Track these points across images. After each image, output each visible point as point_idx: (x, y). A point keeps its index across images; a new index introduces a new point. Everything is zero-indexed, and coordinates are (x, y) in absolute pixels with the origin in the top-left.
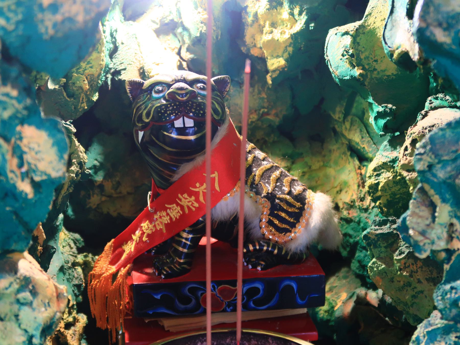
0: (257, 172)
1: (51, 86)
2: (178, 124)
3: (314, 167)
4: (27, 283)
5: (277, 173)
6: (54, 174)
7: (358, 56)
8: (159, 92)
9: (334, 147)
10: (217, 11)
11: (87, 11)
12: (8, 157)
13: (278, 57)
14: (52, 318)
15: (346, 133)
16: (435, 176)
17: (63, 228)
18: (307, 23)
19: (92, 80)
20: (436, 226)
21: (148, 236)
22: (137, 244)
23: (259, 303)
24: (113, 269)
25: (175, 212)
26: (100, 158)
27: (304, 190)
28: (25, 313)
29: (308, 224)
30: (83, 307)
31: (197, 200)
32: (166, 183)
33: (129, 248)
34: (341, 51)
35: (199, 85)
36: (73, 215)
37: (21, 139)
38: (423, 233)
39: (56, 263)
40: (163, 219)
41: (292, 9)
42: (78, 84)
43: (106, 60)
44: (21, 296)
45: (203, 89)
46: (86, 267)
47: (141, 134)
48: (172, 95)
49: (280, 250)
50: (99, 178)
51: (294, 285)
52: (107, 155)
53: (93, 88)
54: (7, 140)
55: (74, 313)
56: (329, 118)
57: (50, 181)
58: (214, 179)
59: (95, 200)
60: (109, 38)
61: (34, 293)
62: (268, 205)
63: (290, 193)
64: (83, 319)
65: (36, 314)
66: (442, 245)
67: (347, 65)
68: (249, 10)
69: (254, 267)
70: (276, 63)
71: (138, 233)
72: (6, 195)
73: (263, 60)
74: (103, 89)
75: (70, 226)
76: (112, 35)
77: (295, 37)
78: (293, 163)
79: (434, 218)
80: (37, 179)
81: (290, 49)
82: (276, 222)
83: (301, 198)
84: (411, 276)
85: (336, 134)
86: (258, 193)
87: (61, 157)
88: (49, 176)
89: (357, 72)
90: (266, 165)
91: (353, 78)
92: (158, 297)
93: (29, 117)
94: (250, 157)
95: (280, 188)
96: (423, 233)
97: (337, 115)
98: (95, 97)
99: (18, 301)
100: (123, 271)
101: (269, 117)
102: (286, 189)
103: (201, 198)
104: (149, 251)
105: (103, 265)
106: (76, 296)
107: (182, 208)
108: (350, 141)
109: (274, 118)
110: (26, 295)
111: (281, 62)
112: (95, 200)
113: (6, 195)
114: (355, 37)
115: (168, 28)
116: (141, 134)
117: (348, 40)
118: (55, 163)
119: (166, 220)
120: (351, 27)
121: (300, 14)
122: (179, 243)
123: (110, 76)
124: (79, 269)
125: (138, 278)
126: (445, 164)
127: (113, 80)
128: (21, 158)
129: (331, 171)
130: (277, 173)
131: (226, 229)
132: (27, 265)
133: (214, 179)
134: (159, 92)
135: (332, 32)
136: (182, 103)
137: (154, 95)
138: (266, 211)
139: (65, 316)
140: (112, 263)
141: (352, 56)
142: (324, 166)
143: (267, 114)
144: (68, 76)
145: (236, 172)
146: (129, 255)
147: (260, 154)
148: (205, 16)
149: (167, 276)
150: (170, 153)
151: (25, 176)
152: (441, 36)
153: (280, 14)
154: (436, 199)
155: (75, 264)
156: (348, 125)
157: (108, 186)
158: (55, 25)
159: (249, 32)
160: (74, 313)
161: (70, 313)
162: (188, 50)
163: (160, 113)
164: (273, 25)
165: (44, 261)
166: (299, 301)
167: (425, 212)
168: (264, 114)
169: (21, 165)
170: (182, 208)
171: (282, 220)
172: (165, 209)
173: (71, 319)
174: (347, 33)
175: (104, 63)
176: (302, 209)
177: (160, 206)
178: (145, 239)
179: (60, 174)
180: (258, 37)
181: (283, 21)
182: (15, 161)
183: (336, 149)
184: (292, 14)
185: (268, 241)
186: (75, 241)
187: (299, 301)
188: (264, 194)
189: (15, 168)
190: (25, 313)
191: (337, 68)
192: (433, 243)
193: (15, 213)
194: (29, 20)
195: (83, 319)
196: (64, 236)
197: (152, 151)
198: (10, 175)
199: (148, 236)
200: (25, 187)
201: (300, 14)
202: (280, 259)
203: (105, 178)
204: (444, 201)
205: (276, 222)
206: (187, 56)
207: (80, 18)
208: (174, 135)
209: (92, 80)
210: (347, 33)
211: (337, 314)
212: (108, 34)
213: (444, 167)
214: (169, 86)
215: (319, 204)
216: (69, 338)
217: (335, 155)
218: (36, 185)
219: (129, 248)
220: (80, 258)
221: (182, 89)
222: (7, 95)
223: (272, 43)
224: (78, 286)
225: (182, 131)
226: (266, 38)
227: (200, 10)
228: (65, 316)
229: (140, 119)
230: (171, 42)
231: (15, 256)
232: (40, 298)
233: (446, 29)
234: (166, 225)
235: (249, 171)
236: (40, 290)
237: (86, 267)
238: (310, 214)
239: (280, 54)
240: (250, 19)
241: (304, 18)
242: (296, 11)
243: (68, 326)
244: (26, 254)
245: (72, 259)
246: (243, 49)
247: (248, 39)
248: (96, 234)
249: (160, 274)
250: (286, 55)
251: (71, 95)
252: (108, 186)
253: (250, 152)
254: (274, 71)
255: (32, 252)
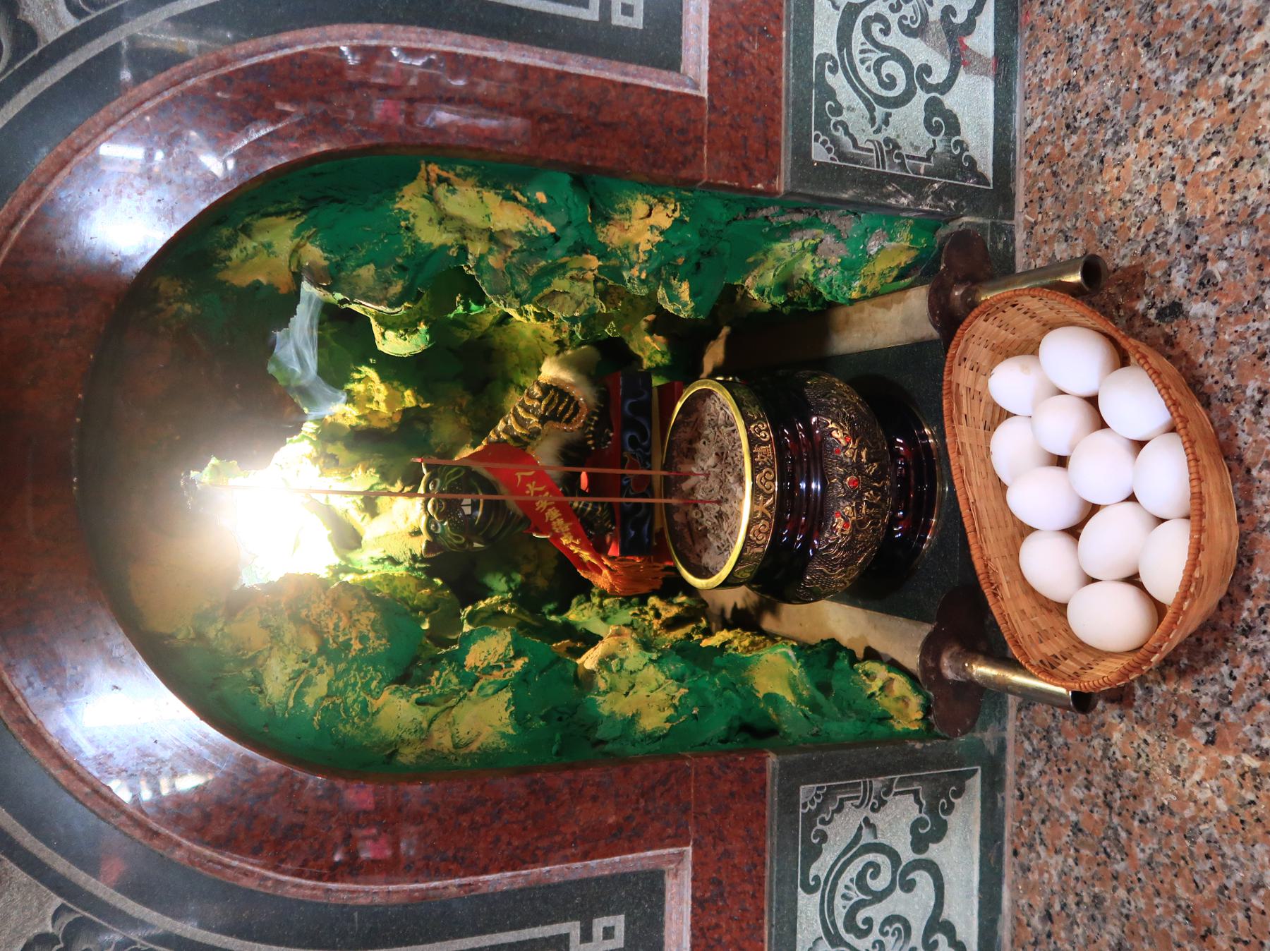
0: (518, 430)
1: (426, 626)
2: (468, 511)
3: (517, 362)
4: (604, 663)
5: (520, 410)
6: (509, 639)
7: (406, 324)
8: (436, 527)
9: (497, 339)
10: (354, 456)
11: (366, 609)
12: (492, 679)
13: (403, 397)
14: (636, 641)
15: (484, 328)
16: (526, 292)
17: (565, 616)
18: (370, 365)
19: (422, 585)
20: (572, 291)
21: (575, 538)
22: (582, 549)
23: (644, 436)
24: (605, 572)
25: (553, 514)
26: (499, 576)
27: (538, 383)
28: (629, 665)
29: (570, 384)
30: (643, 601)
31: (543, 492)
32: (525, 520)
33: (586, 556)
34: (400, 341)
35: (431, 487)
36: (663, 354)
37: (476, 668)
38: (579, 304)
39: (596, 627)
40: (559, 524)
41: (354, 381)
42: (425, 599)
43: (400, 571)
44: (614, 669)
45: (435, 485)
46: (603, 595)
47: (476, 545)
48: (439, 515)
49: (594, 414)
50: (518, 578)
51: (629, 402)
52: (496, 569)
53: (428, 583)
54: (477, 680)
55: (647, 609)
56: (468, 343)
57: (515, 641)
58: (523, 477)
59: (541, 582)
60: (379, 566)
61: (613, 657)
62: (550, 422)
63: (540, 400)
64: (653, 600)
65: (631, 656)
66: (590, 288)
67: (415, 336)
68: (354, 424)
69: (610, 439)
70: (409, 399)
71: (572, 548)
72: (525, 680)
73: (406, 411)
74: (430, 573)
75: (564, 608)
76: (376, 563)
77: (383, 379)
78: (512, 382)
79: (565, 292)
80: (512, 654)
81: (396, 384)
82: (567, 416)
83: (546, 389)
84: (622, 299)
85: (485, 336)
86: (538, 432)
87: (494, 633)
88: (509, 644)
89: (423, 327)
90: (511, 421)
91: (428, 332)
92: (633, 533)
93: (457, 659)
94: (504, 436)
95: (535, 409)
96: (579, 304)
97: (465, 336)
98: (439, 582)
99: (618, 671)
100: (606, 562)
101: (464, 404)
102: (536, 403)
103: (541, 489)
104: (590, 537)
105: (603, 580)
106: (631, 606)
107: (549, 507)
108: (492, 324)
109: (466, 400)
110: (614, 664)
111: (408, 393)
112: (541, 582)
113: (525, 680)
114: (387, 327)
115: (370, 503)
116: (476, 545)
117: (390, 334)
118: (499, 638)
119: (560, 522)
120: (376, 329)
121: (360, 372)
122: (583, 510)
123: (417, 565)
124: (606, 602)
125: (614, 551)
126: (514, 283)
127: (421, 562)
128: (493, 668)
129: (522, 345)
130: (520, 410)
131: (573, 454)
132: (589, 660)
133: (523, 477)
134: (436, 527)
135: (380, 347)
136: (447, 509)
137: (439, 531)
138: (557, 425)
139: (648, 618)
140: (600, 572)
141: (406, 331)
142: (516, 350)
143: (461, 406)
144: (416, 609)
145: (517, 449)
146: (592, 556)
147: (501, 425)
148: (359, 470)
149: (613, 523)
150: (496, 517)
151: (508, 664)
152: (397, 288)
153: (359, 393)
154: (546, 291)
155: (601, 606)
156: (475, 326)
157: (528, 568)
158: (378, 638)
159: (376, 424)
160: (647, 609)
161: (646, 613)
162: (393, 484)
163: (455, 526)
164: (370, 399)
165: (591, 640)
166: (645, 397)
167: (559, 299)
168: (461, 410)
169: (500, 668)
170: (549, 507)
171: (566, 409)
172: (550, 522)
173: (652, 613)
174: (383, 334)
175: (405, 573)
176: (557, 389)
177: (547, 527)
178: (577, 542)
179: (508, 634)
180: (381, 416)
181: (367, 390)
182: (495, 672)
183: (499, 338)
184: (359, 381)
185: (585, 425)
186: (580, 603)
187: (645, 397)
188: (539, 426)
189: (502, 673)
190: (629, 665)
191: (417, 346)
192: (588, 295)
193: (542, 672)
194: (373, 661)
195: (653, 600)
196: (572, 616)
197: (495, 532)
198: (507, 677)
199: (575, 538)
200: (519, 664)
201: (360, 372)
202: (604, 412)
203: (519, 572)
204: (549, 285)
205: (567, 416)
206: (398, 486)
207: (372, 615)
208: (479, 513)
209: (422, 585)
210: (383, 334)
211: (664, 348)
212: (376, 567)
213: (518, 284)
214: (430, 517)
215: (550, 371)
216: (669, 615)
217: (506, 339)
218: (517, 656)
219: (586, 556)
220: (596, 600)
221: (434, 507)
222: (438, 680)
223: (389, 402)
224: (622, 604)
225: (475, 506)
226: (383, 408)
227: (353, 475)
228: (648, 618)
229: (462, 546)
230: (382, 501)
231: (580, 672)
232: (618, 652)
233: (390, 283)
234: (566, 521)
235: (516, 438)
236: (611, 651)
237: (603, 595)
238: (562, 381)
239: (399, 394)
240: (363, 423)
241: (364, 369)
242: (356, 376)
243: (658, 615)
244: (579, 661)
245: (595, 609)
246: (394, 429)
247: (384, 425)
248: (573, 586)
249: (610, 530)
250: (402, 388)
251: (436, 606)
252: (528, 568)
253: (498, 436)
254: (417, 400)
255: (580, 653)
